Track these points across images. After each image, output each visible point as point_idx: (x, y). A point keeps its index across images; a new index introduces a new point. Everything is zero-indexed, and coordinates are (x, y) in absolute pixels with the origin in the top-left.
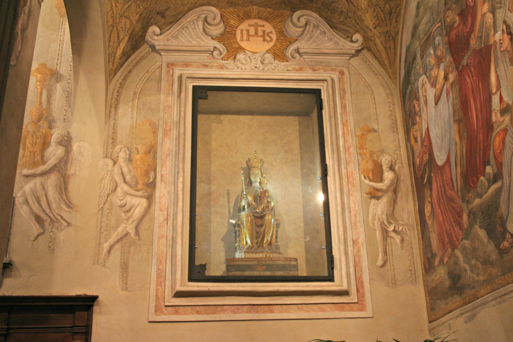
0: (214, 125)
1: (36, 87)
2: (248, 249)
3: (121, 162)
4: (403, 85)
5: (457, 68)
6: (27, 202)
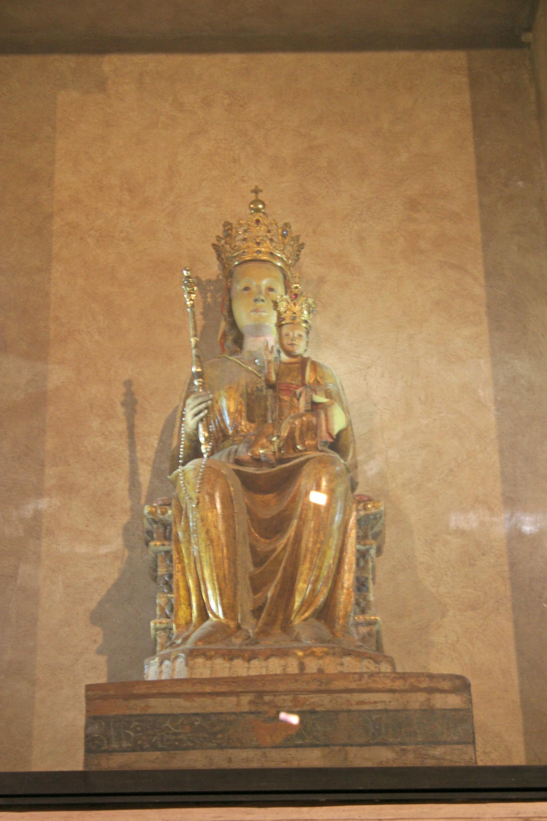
2: (206, 638)
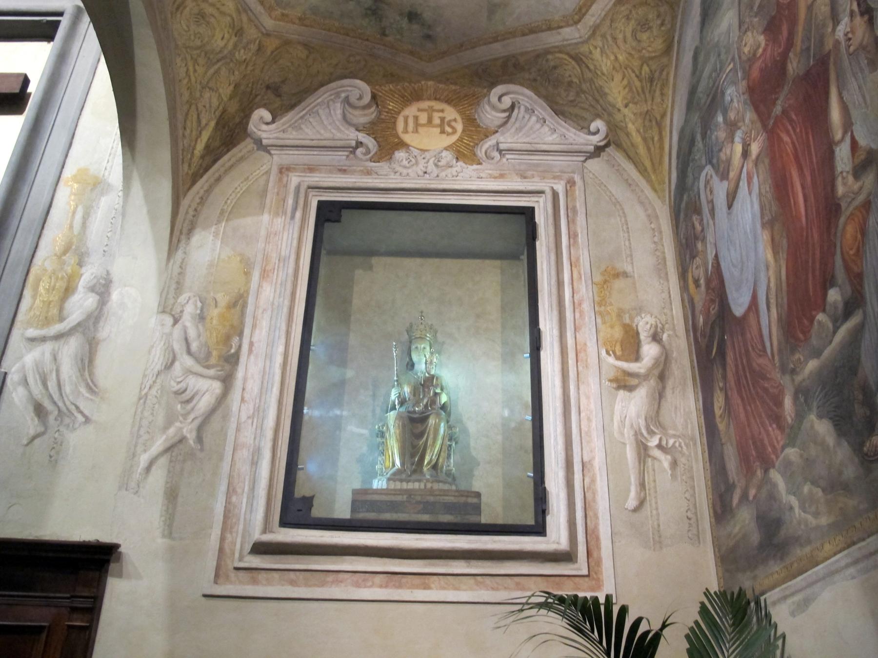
0: (359, 272)
1: (68, 203)
2: (394, 474)
3: (187, 320)
4: (675, 200)
5: (764, 126)
6: (25, 382)
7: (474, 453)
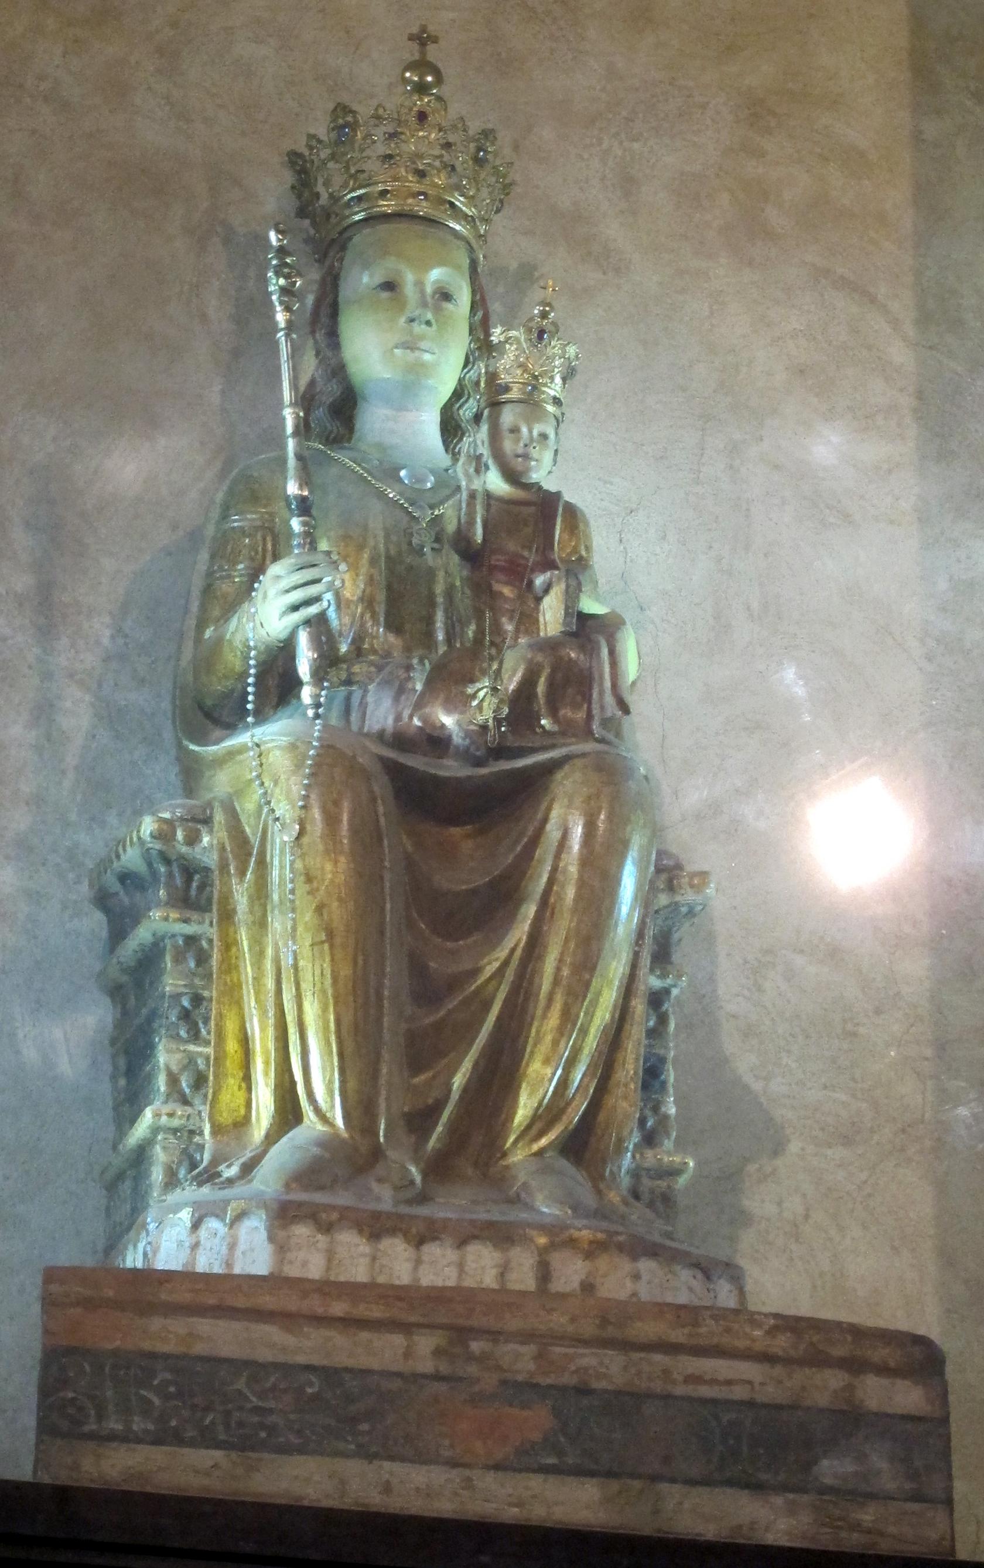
2: (309, 1175)
7: (744, 1063)
